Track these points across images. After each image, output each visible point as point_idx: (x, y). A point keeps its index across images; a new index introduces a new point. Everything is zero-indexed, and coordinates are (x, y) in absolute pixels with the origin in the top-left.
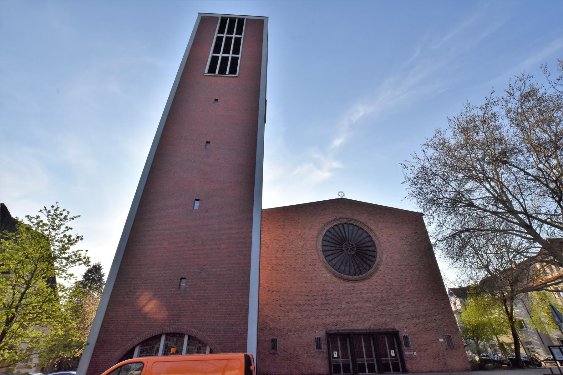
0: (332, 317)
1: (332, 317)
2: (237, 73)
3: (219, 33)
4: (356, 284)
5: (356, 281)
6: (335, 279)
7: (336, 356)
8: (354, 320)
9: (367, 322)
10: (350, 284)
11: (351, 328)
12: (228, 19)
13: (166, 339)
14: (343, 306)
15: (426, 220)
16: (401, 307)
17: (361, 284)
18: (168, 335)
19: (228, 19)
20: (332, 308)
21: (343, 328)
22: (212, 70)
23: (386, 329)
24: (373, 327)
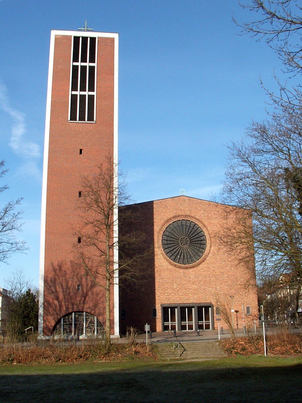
0: (166, 295)
1: (166, 295)
2: (95, 120)
3: (74, 61)
4: (186, 271)
5: (186, 268)
6: (170, 267)
7: (279, 308)
8: (182, 297)
9: (191, 298)
10: (182, 271)
11: (179, 302)
12: (81, 38)
13: (75, 314)
14: (175, 287)
15: (119, 336)
16: (218, 287)
17: (190, 270)
18: (75, 312)
19: (81, 38)
20: (167, 289)
21: (173, 303)
22: (73, 118)
23: (205, 303)
24: (195, 302)
